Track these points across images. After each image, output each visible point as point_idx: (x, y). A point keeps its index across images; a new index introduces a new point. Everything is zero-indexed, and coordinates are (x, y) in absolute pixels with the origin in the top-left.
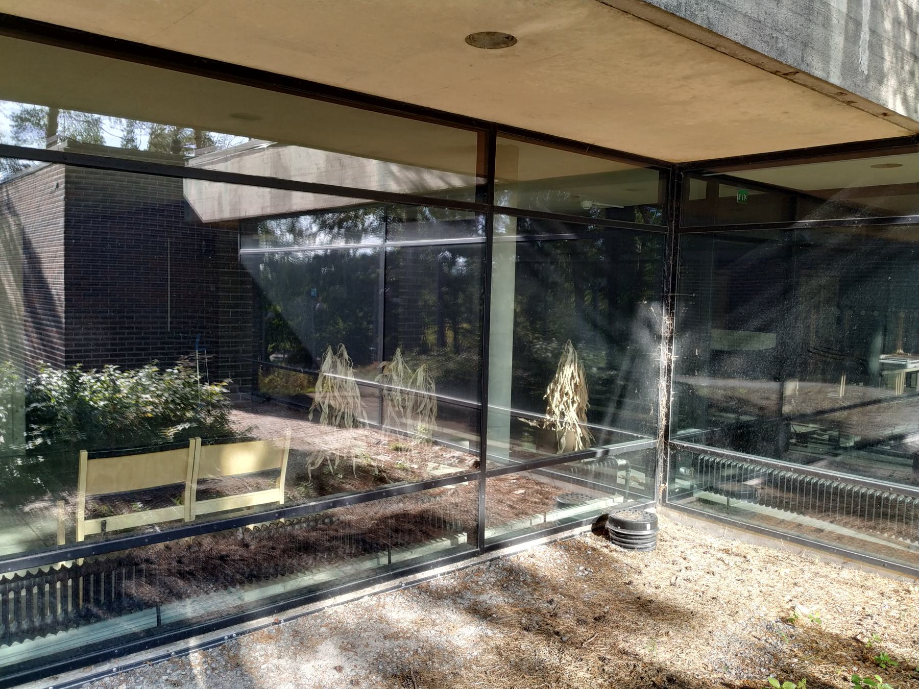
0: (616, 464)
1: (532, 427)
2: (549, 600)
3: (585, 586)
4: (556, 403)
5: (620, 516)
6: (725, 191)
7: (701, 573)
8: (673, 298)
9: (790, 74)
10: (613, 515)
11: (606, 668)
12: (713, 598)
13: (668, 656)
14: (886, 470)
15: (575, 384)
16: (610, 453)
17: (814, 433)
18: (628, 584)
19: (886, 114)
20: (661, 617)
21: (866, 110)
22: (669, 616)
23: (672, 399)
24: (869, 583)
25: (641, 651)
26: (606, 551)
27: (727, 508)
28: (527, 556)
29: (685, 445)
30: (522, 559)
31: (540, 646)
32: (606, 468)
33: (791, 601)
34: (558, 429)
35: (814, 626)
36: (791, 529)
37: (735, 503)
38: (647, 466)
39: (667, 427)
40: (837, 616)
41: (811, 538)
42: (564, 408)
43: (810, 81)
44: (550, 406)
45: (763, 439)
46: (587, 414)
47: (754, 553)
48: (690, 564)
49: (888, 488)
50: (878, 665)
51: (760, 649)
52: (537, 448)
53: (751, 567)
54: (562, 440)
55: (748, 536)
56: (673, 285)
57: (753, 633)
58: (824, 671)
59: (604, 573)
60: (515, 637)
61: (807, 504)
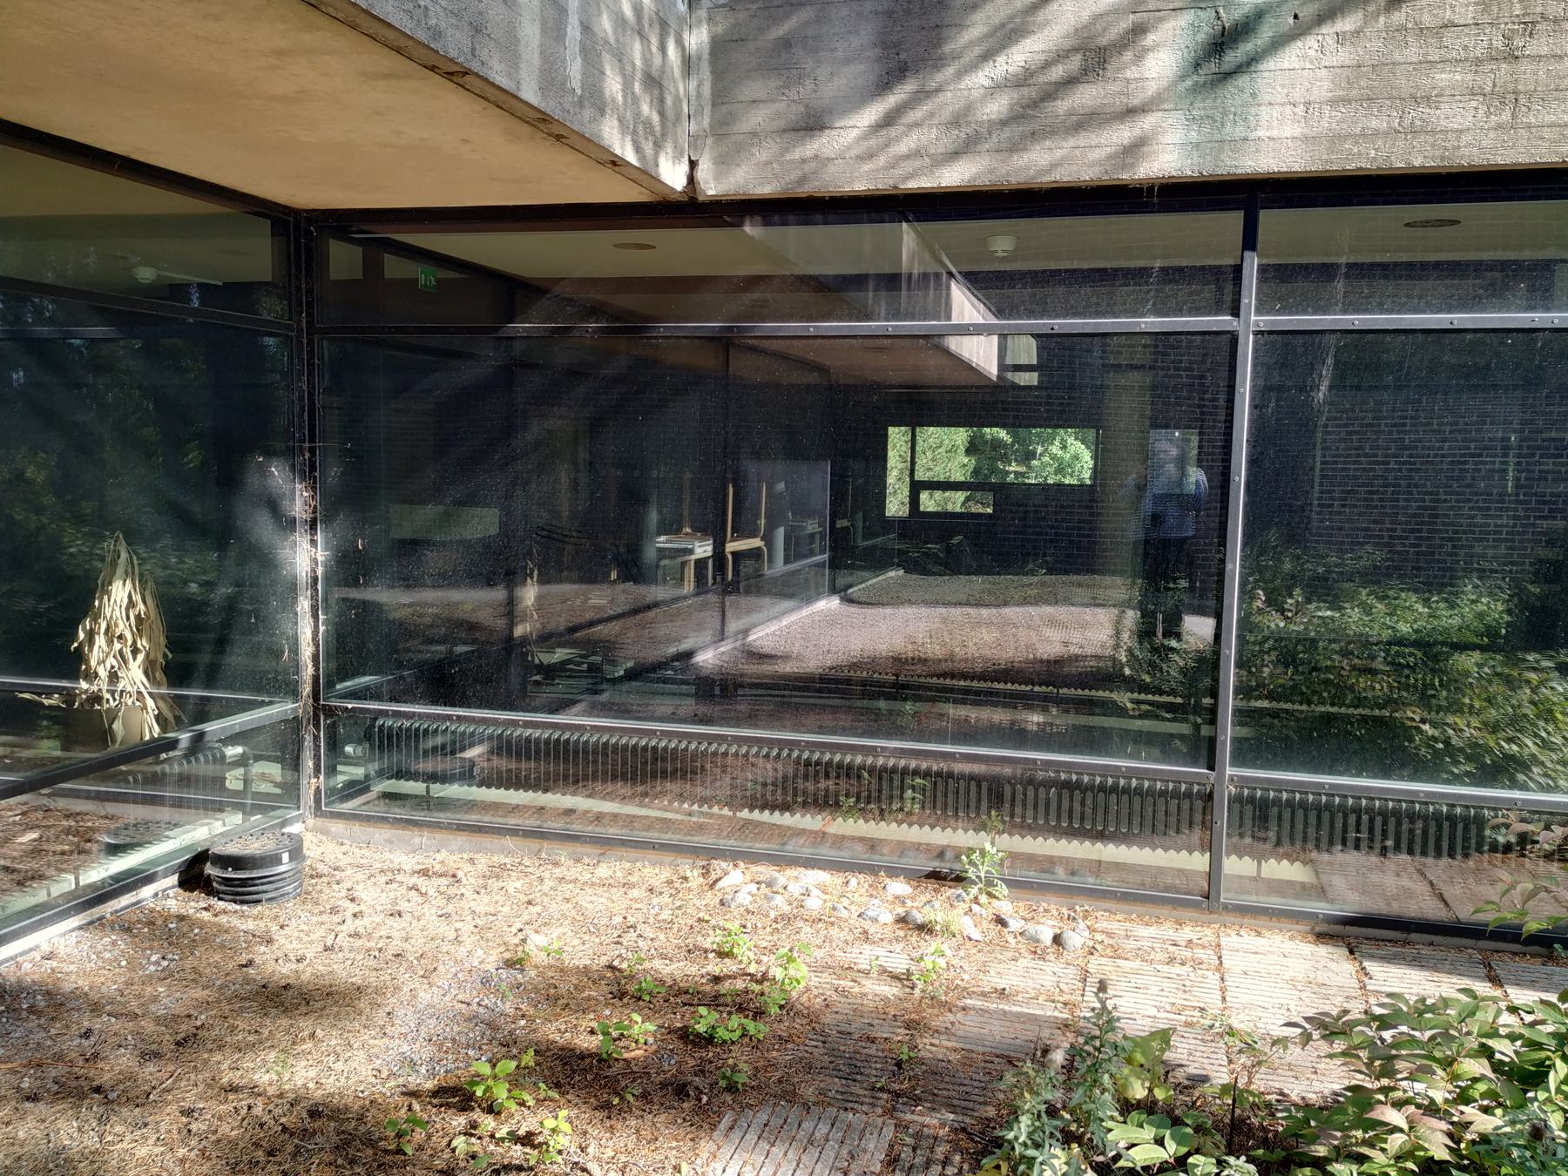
0: (223, 756)
1: (50, 707)
2: (83, 1031)
3: (161, 989)
4: (100, 655)
5: (233, 849)
6: (395, 267)
7: (378, 919)
8: (312, 451)
9: (457, 75)
10: (218, 849)
11: (194, 1127)
12: (398, 955)
13: (312, 1073)
14: (665, 706)
15: (138, 617)
16: (207, 738)
17: (568, 662)
18: (246, 966)
19: (616, 163)
20: (303, 1009)
21: (586, 152)
22: (318, 1005)
23: (322, 628)
24: (633, 879)
25: (263, 1078)
26: (206, 916)
27: (426, 802)
28: (39, 958)
29: (350, 706)
30: (27, 966)
31: (60, 1124)
32: (211, 767)
33: (521, 930)
34: (106, 706)
35: (552, 962)
36: (529, 818)
37: (439, 790)
38: (283, 753)
39: (316, 678)
40: (587, 938)
41: (556, 825)
42: (115, 663)
43: (490, 92)
44: (87, 662)
45: (475, 680)
46: (166, 670)
47: (467, 867)
48: (363, 907)
49: (654, 732)
50: (639, 999)
51: (469, 1020)
52: (64, 749)
53: (463, 891)
54: (115, 726)
55: (461, 839)
56: (312, 429)
57: (460, 997)
58: (563, 1027)
59: (208, 958)
60: (6, 1120)
61: (547, 773)
